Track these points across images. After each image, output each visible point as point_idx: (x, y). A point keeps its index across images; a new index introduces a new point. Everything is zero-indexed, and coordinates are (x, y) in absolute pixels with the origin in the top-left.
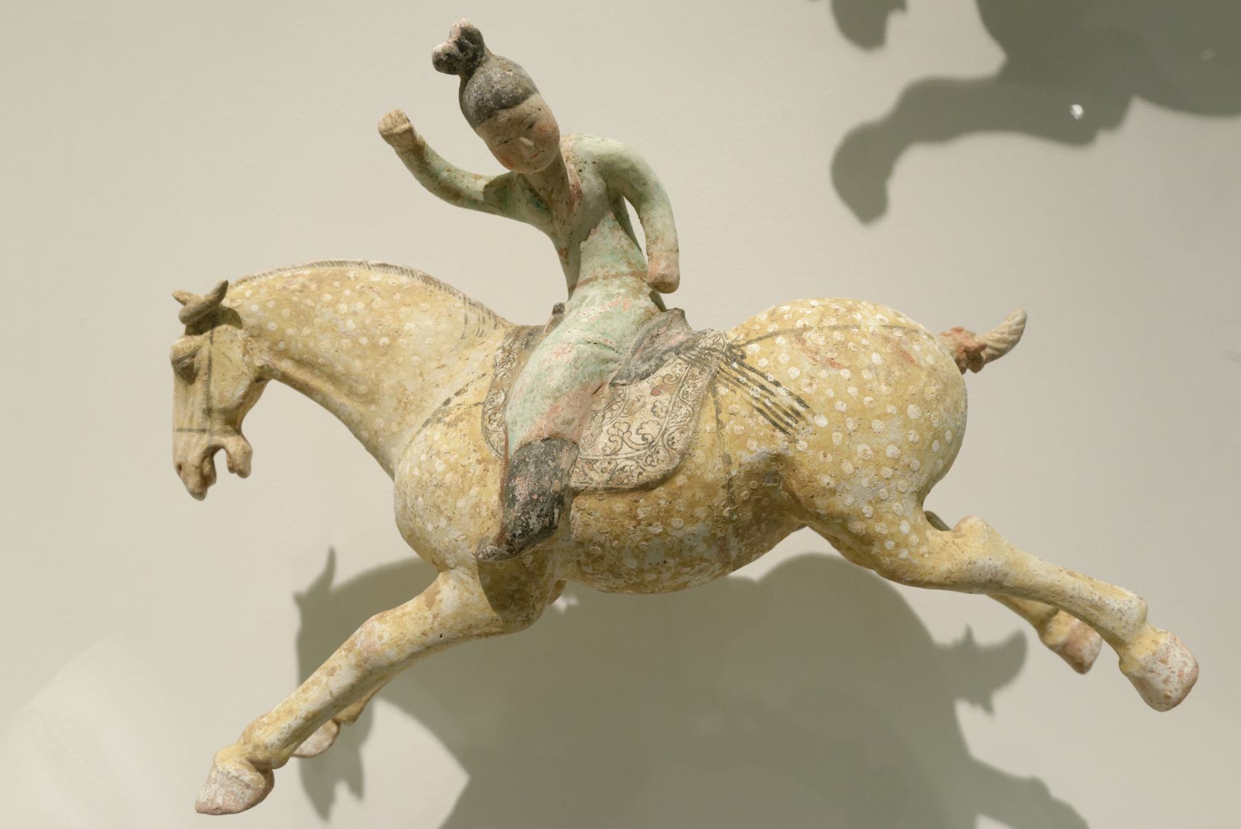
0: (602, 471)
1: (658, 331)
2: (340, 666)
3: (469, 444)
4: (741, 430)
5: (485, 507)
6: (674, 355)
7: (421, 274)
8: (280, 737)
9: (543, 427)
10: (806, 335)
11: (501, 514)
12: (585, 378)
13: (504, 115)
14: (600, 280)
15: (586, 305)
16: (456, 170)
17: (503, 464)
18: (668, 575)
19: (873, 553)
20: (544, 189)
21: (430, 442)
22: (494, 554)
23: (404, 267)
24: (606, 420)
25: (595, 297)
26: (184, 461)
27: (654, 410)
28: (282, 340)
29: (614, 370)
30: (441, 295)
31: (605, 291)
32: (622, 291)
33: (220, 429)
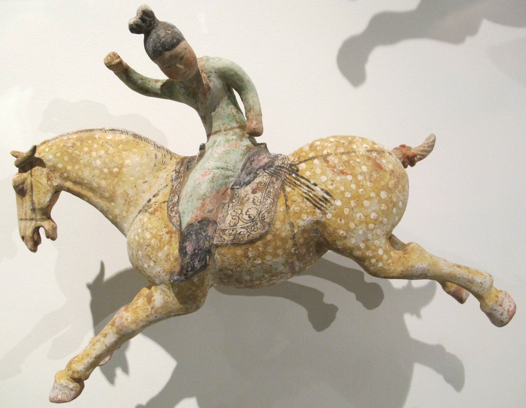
0: (229, 235)
1: (254, 158)
2: (109, 333)
3: (162, 224)
4: (299, 209)
5: (172, 256)
6: (262, 170)
7: (132, 133)
8: (84, 367)
9: (198, 215)
10: (329, 158)
11: (180, 260)
12: (218, 187)
13: (167, 54)
14: (223, 132)
15: (216, 146)
16: (146, 78)
17: (180, 234)
18: (265, 281)
19: (365, 265)
20: (191, 87)
21: (142, 223)
22: (178, 280)
23: (123, 130)
24: (230, 208)
25: (220, 141)
26: (25, 235)
27: (254, 202)
28: (65, 172)
29: (233, 181)
30: (142, 144)
31: (225, 138)
32: (234, 137)
33: (40, 218)
